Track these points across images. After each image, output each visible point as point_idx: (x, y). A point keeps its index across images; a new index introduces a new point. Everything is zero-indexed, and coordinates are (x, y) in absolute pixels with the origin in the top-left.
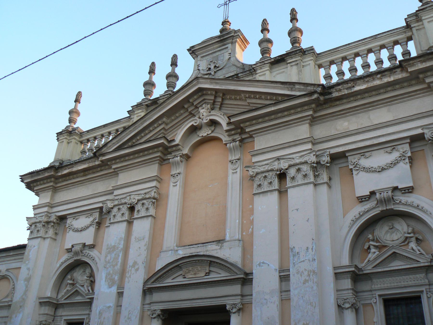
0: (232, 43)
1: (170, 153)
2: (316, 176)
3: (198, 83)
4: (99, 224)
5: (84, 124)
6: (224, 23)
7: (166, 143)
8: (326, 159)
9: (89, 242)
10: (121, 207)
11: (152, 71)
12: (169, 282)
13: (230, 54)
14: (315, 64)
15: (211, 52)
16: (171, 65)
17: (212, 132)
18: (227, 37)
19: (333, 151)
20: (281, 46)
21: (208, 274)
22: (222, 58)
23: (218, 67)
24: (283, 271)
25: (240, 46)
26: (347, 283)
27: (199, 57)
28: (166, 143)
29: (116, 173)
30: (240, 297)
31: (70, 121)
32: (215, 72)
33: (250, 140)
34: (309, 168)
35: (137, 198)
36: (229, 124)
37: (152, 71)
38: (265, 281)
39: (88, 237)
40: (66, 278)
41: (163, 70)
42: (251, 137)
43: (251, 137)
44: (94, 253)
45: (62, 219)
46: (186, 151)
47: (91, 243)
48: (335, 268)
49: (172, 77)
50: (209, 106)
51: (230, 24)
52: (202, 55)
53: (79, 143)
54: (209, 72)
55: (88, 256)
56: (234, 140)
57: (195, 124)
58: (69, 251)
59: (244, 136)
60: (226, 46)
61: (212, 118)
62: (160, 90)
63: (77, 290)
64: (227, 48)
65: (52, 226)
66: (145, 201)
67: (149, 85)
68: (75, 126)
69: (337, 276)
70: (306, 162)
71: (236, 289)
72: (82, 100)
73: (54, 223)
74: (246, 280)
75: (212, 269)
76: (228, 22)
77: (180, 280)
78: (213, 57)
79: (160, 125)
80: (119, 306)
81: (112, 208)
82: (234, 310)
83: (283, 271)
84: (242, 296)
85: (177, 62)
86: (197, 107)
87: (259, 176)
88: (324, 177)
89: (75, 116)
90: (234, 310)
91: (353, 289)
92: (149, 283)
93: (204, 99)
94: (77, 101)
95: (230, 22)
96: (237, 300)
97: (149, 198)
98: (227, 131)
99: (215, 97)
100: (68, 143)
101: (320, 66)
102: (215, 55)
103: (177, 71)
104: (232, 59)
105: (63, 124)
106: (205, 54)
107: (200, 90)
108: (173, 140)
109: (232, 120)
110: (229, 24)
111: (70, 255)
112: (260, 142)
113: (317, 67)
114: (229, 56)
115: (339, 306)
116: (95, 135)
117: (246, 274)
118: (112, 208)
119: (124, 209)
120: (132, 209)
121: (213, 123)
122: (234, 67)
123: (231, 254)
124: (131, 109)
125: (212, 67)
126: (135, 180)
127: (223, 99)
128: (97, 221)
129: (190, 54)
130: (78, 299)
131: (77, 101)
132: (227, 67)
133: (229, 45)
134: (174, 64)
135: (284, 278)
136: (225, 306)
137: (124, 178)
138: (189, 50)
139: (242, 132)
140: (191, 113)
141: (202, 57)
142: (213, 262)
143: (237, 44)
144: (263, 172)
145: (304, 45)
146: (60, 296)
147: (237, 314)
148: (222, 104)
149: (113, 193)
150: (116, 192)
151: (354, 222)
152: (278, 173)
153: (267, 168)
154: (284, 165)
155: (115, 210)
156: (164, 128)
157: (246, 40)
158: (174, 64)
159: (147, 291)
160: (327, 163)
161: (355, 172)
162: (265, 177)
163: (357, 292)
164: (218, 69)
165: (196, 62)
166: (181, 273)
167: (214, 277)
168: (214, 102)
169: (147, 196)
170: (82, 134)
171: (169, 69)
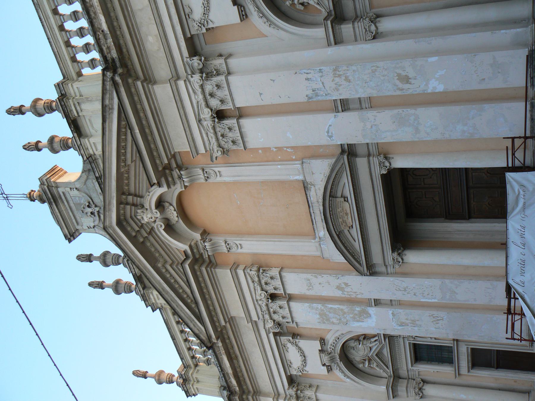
0: (57, 187)
1: (201, 255)
2: (218, 74)
3: (111, 227)
4: (295, 335)
5: (173, 364)
6: (32, 199)
7: (189, 261)
8: (196, 62)
9: (317, 345)
10: (271, 310)
11: (100, 285)
12: (358, 245)
13: (71, 189)
14: (77, 80)
15: (71, 213)
16: (91, 261)
17: (171, 205)
18: (49, 194)
19: (186, 53)
20: (57, 125)
21: (346, 199)
22: (77, 199)
23: (89, 203)
24: (336, 107)
25: (60, 177)
26: (346, 29)
27: (78, 227)
28: (189, 261)
29: (231, 320)
30: (371, 158)
31: (170, 381)
32: (96, 206)
33: (178, 158)
34: (209, 82)
35: (259, 291)
36: (159, 185)
37: (100, 285)
38: (350, 129)
39: (311, 348)
40: (363, 369)
41: (97, 271)
42: (174, 156)
43: (174, 156)
44: (330, 338)
45: (291, 380)
46: (197, 236)
47: (318, 342)
48: (329, 45)
49: (106, 259)
50: (139, 211)
51: (32, 191)
52: (75, 224)
53: (197, 368)
54: (96, 214)
55: (334, 345)
56: (180, 177)
57: (163, 227)
58: (330, 369)
59: (174, 165)
60: (62, 194)
61: (153, 207)
62: (125, 275)
63: (376, 355)
64: (63, 193)
65: (301, 392)
66: (263, 282)
67: (118, 287)
68: (177, 375)
69: (338, 41)
70: (202, 86)
71: (361, 163)
72: (143, 369)
73: (297, 390)
74: (349, 152)
75: (339, 194)
76: (30, 194)
77: (356, 232)
78: (77, 209)
79: (167, 270)
80: (391, 303)
81: (274, 321)
82: (387, 164)
83: (336, 107)
84: (369, 155)
85: (87, 255)
86: (142, 226)
87: (222, 143)
88: (219, 62)
89: (164, 377)
90: (387, 164)
91: (353, 22)
92: (361, 269)
93: (131, 217)
94: (144, 375)
95: (29, 191)
96: (375, 161)
97: (258, 276)
98: (169, 187)
99: (127, 204)
100: (198, 381)
101: (79, 74)
102: (74, 208)
103: (97, 253)
104: (77, 186)
105: (175, 390)
106: (74, 221)
107: (119, 223)
108: (185, 252)
109: (155, 181)
110: (32, 193)
111: (334, 367)
112: (180, 144)
113: (80, 78)
114: (75, 189)
115: (374, 38)
116: (186, 350)
117: (343, 152)
118: (274, 321)
119: (274, 306)
120: (273, 297)
121: (160, 204)
122: (88, 183)
123: (319, 172)
124: (150, 307)
125: (90, 210)
126: (236, 295)
127: (130, 194)
128: (291, 338)
129: (74, 239)
130: (386, 352)
131: (144, 375)
132: (88, 192)
133: (60, 190)
134: (89, 258)
135: (344, 106)
136: (383, 176)
137: (236, 309)
138: (70, 241)
139: (169, 168)
140: (150, 233)
141: (78, 224)
142: (331, 194)
143: (58, 181)
144: (217, 140)
145: (54, 96)
146: (385, 375)
147: (391, 161)
148: (136, 195)
149: (256, 322)
150: (255, 318)
151: (271, 24)
152: (216, 120)
153: (211, 135)
154: (206, 114)
155: (275, 317)
156: (171, 265)
157: (53, 169)
158: (89, 258)
159: (371, 270)
160: (201, 60)
161: (211, 25)
162: (223, 136)
163: (357, 17)
164: (91, 203)
165: (85, 231)
166: (346, 232)
167: (348, 191)
168: (133, 205)
169: (256, 279)
170: (186, 366)
171: (96, 264)
